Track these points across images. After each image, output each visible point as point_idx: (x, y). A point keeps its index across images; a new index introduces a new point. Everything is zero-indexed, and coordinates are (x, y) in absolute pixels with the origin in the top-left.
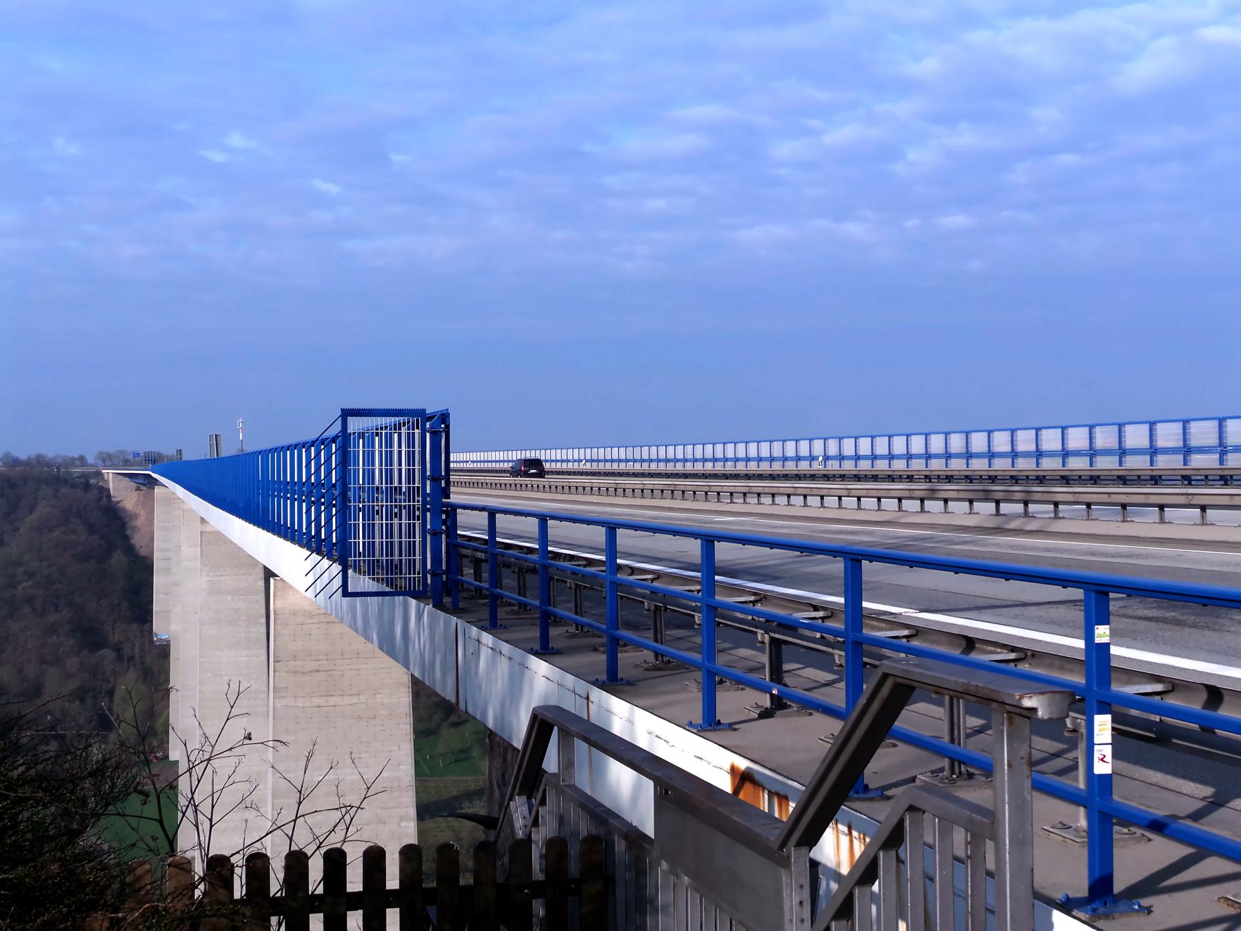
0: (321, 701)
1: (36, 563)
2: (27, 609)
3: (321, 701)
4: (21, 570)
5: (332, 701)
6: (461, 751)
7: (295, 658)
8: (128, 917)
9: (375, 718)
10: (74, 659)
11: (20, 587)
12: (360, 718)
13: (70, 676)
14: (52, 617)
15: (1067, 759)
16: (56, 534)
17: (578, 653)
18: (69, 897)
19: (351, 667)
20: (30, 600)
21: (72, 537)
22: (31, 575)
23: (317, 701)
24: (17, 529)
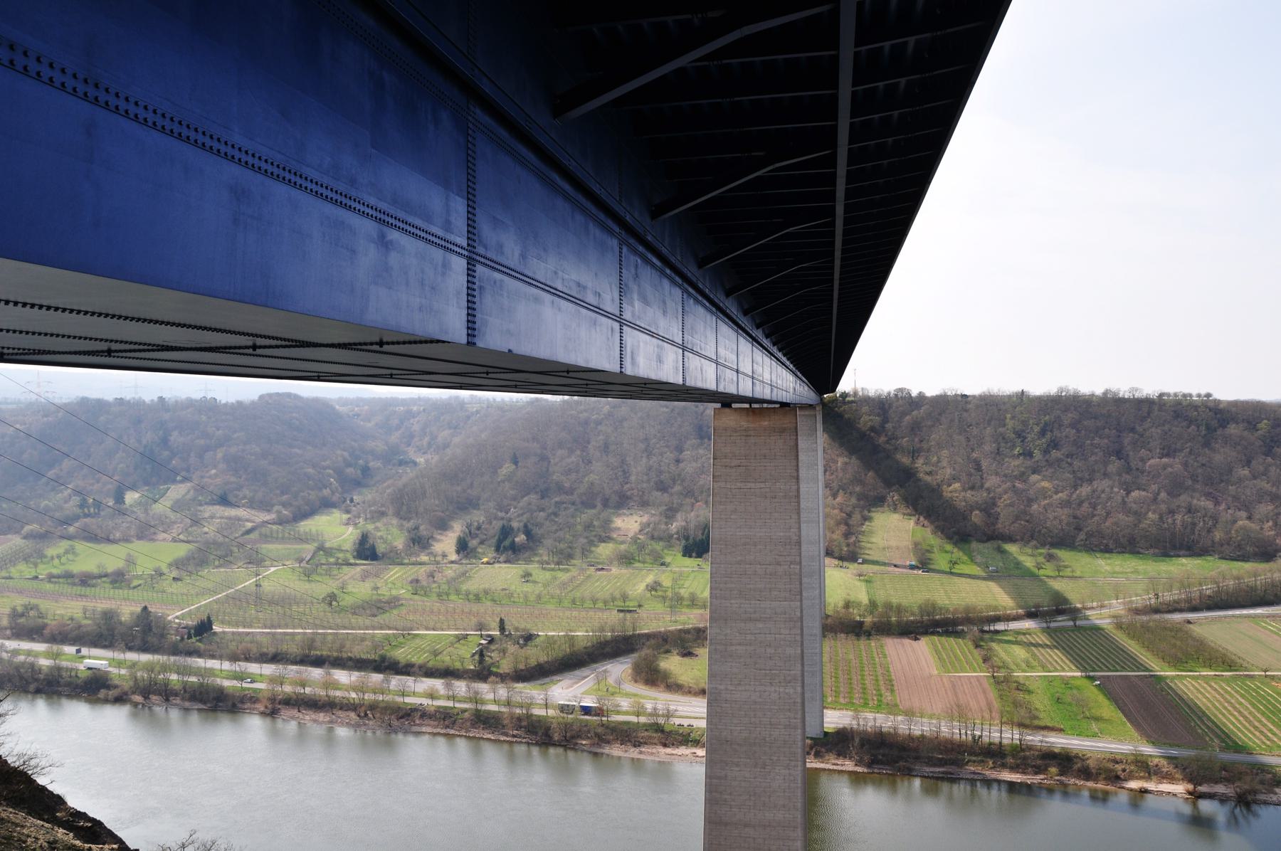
5: (749, 485)
7: (726, 457)
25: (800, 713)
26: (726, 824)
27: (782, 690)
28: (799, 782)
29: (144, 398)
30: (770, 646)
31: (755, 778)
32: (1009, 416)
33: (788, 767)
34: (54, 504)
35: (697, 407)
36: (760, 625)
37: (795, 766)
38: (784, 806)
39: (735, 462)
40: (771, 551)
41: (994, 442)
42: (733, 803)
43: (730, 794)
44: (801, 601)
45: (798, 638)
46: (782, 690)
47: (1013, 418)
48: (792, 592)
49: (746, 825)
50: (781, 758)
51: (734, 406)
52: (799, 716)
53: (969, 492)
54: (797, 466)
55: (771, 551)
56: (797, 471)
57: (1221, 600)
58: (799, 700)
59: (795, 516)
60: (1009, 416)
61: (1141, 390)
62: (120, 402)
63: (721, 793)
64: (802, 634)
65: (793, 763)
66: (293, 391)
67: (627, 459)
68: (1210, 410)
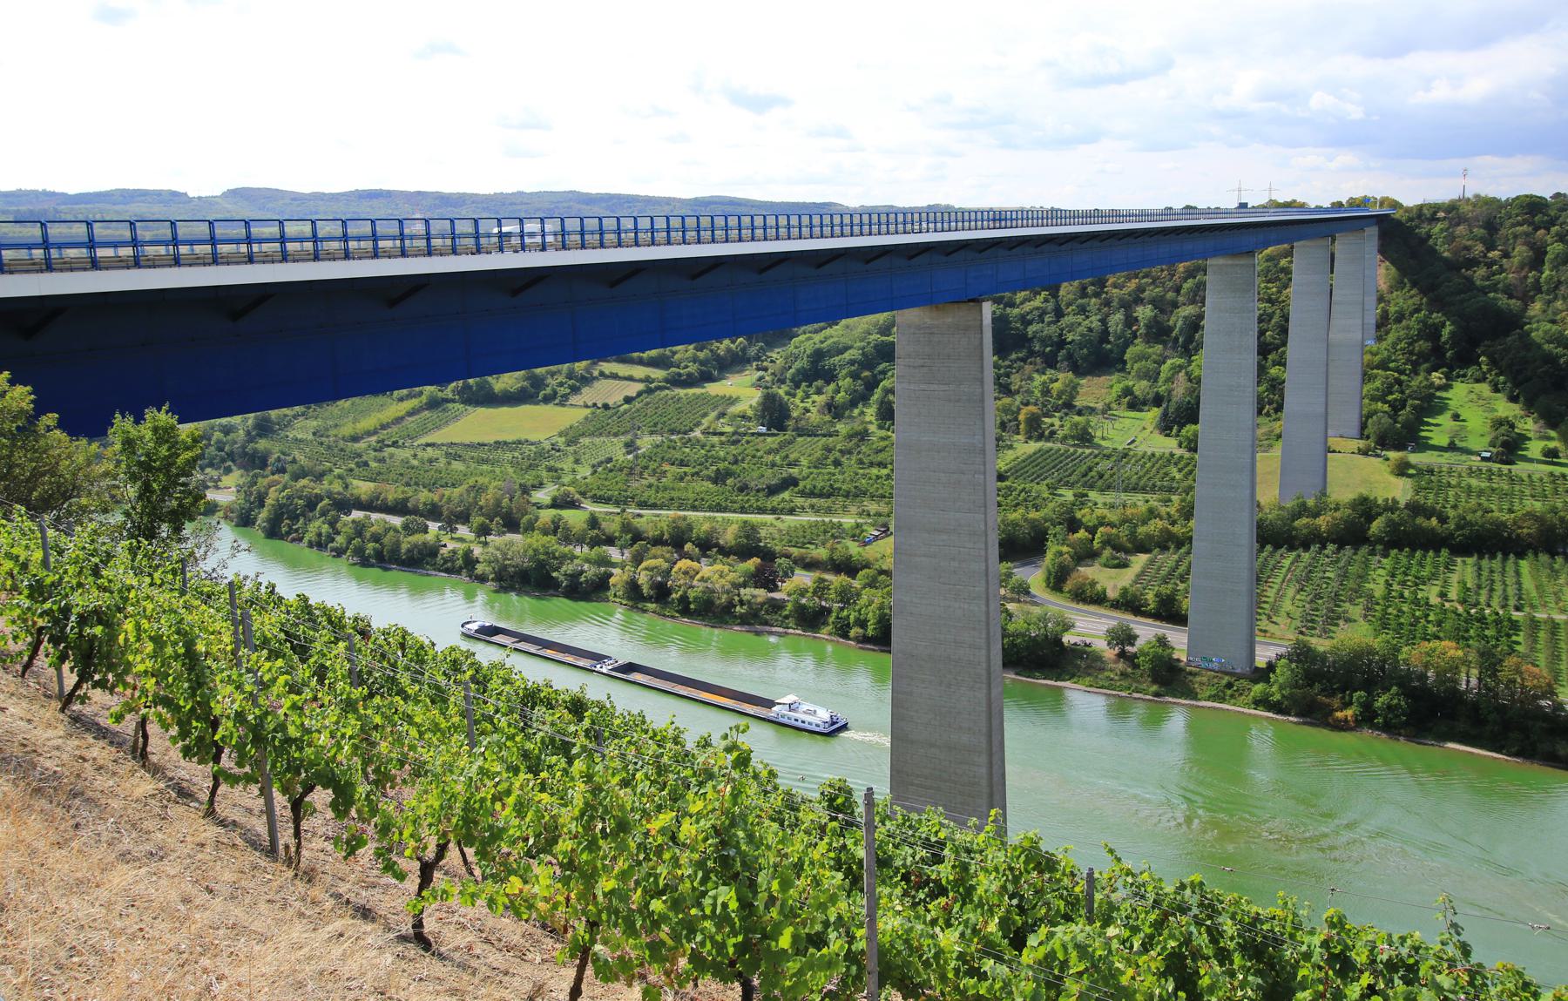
5: (933, 387)
25: (984, 632)
27: (966, 606)
30: (954, 559)
36: (945, 537)
38: (969, 729)
39: (920, 362)
41: (1324, 547)
44: (985, 514)
45: (983, 553)
46: (966, 606)
52: (984, 636)
54: (982, 367)
56: (982, 372)
57: (1513, 701)
58: (983, 619)
59: (978, 336)
62: (200, 198)
64: (986, 549)
67: (436, 805)
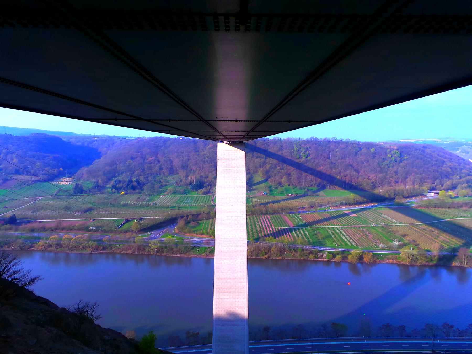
0: (227, 168)
1: (209, 155)
2: (207, 163)
3: (227, 168)
4: (206, 156)
5: (229, 168)
6: (282, 192)
7: (222, 159)
8: (163, 183)
9: (238, 172)
10: (214, 172)
11: (206, 159)
12: (235, 172)
13: (213, 175)
14: (211, 164)
15: (270, 121)
16: (212, 150)
17: (460, 226)
18: (296, 257)
19: (233, 161)
20: (207, 161)
21: (215, 150)
22: (208, 157)
23: (226, 168)
24: (206, 149)
26: (221, 279)
28: (245, 264)
29: (356, 140)
31: (231, 263)
32: (295, 146)
33: (241, 259)
34: (441, 239)
35: (250, 141)
37: (244, 259)
38: (240, 272)
40: (236, 190)
42: (224, 272)
43: (223, 269)
47: (297, 147)
48: (243, 203)
49: (228, 279)
50: (239, 256)
51: (224, 142)
53: (38, 152)
55: (236, 190)
60: (295, 146)
61: (336, 139)
63: (220, 268)
65: (243, 258)
66: (330, 136)
68: (357, 145)
